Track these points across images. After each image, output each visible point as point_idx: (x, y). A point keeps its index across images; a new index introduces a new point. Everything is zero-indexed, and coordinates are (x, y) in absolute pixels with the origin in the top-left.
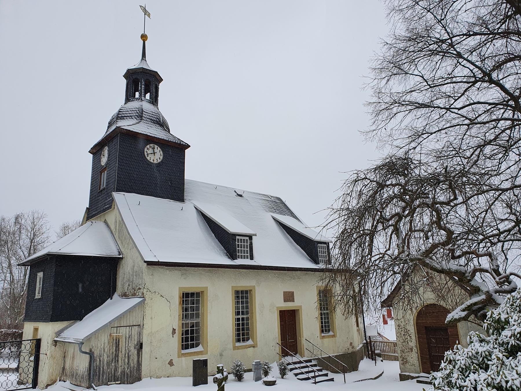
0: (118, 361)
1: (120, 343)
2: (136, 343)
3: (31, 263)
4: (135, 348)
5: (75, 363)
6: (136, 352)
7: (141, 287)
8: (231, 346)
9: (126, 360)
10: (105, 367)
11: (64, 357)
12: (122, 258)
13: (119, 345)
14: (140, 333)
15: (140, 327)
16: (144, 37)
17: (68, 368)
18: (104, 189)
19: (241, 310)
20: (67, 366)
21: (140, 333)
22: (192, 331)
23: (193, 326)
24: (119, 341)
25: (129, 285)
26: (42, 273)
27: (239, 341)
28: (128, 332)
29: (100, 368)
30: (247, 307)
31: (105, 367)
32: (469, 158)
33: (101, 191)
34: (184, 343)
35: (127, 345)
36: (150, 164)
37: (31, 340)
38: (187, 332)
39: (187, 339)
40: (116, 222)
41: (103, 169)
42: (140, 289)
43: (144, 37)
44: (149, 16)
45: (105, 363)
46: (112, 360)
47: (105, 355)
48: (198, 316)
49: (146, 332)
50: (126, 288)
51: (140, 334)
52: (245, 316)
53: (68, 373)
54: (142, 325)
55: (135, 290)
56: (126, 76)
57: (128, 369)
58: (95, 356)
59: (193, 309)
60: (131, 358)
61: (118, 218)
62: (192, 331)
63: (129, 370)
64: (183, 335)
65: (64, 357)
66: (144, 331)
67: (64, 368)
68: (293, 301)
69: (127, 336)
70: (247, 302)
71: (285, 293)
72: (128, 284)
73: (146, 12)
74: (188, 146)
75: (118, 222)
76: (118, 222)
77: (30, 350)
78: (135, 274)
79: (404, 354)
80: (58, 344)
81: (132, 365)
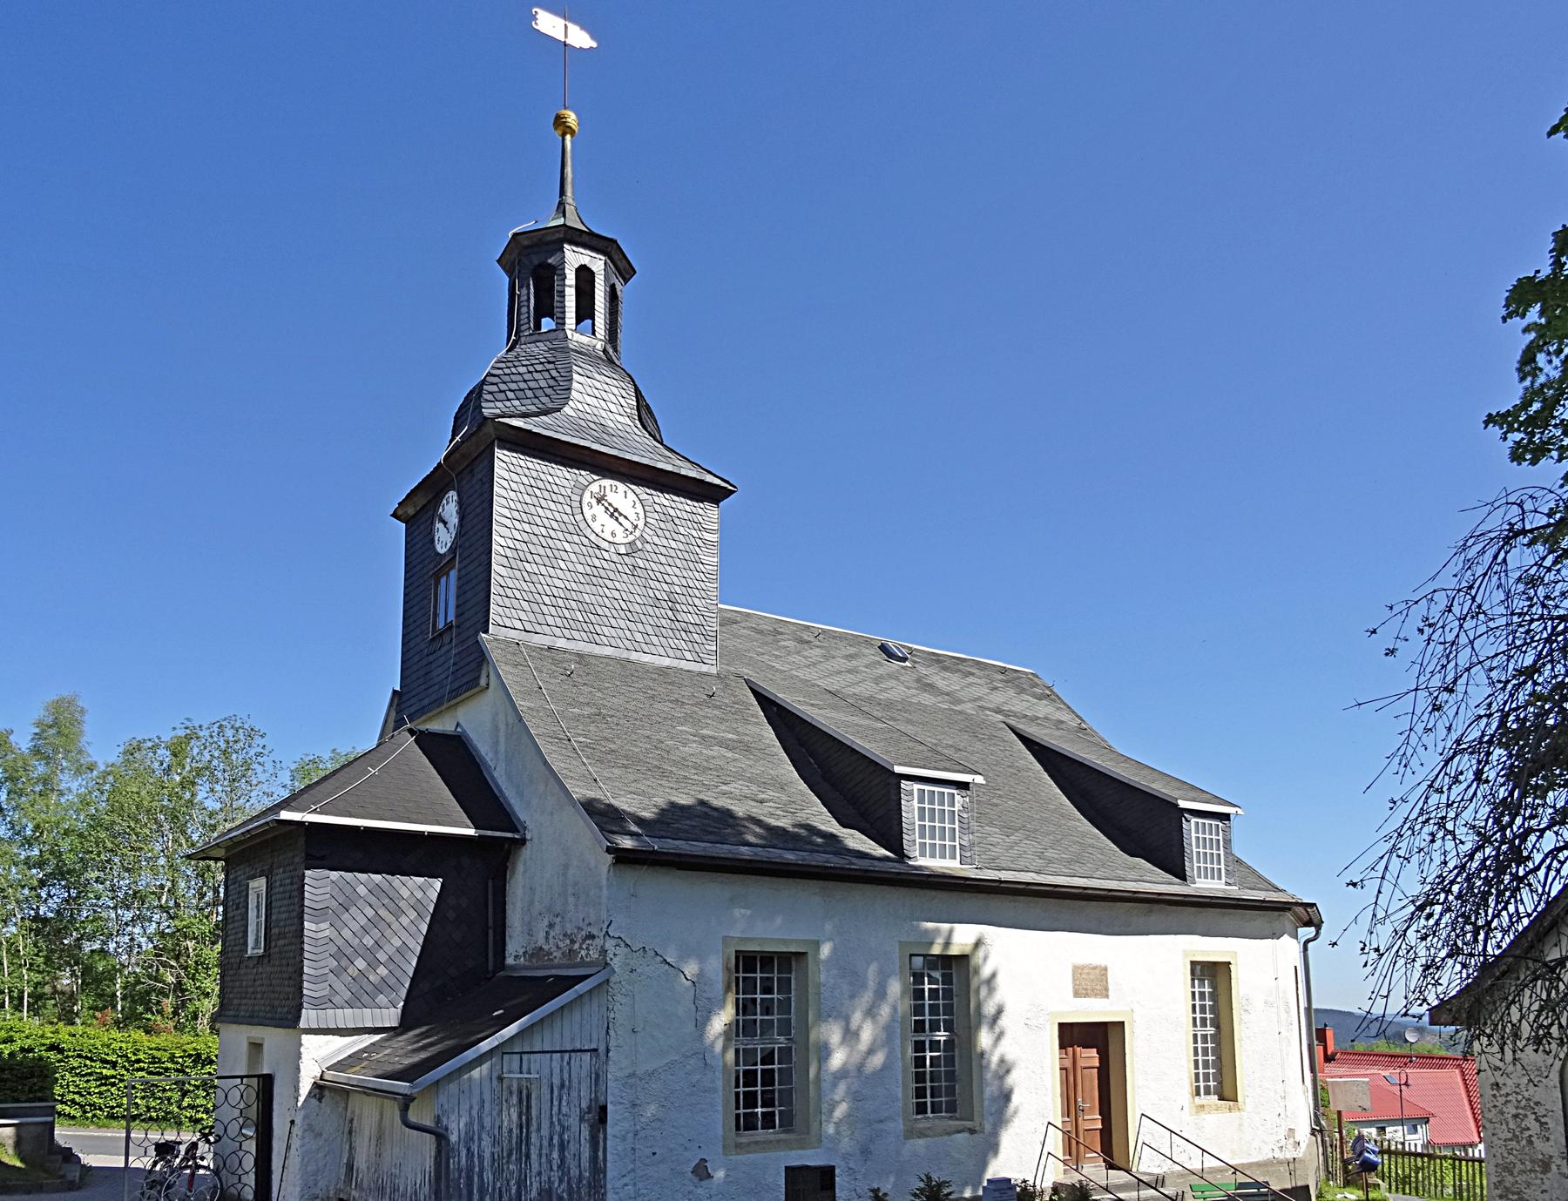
0: (528, 1157)
1: (533, 1103)
2: (584, 1105)
3: (228, 849)
4: (582, 1119)
5: (387, 1156)
6: (586, 1133)
7: (595, 932)
8: (899, 1126)
9: (555, 1155)
10: (488, 1176)
11: (350, 1132)
12: (523, 841)
13: (529, 1107)
14: (597, 1076)
15: (598, 1056)
17: (363, 1166)
18: (449, 627)
19: (927, 1018)
20: (361, 1162)
21: (597, 1076)
22: (768, 1077)
23: (768, 1058)
24: (529, 1097)
25: (551, 926)
26: (262, 882)
27: (921, 1109)
28: (557, 1071)
29: (470, 1179)
31: (488, 1176)
32: (82, 1106)
33: (441, 635)
34: (742, 1111)
35: (555, 1109)
37: (242, 1077)
38: (750, 1078)
39: (750, 1100)
40: (496, 728)
41: (441, 566)
42: (591, 937)
45: (487, 1155)
46: (510, 1155)
47: (484, 1136)
49: (614, 1072)
50: (542, 935)
51: (597, 1078)
53: (365, 1185)
54: (602, 1049)
55: (573, 942)
57: (561, 1181)
58: (453, 1138)
60: (573, 1147)
61: (501, 717)
62: (768, 1077)
63: (564, 1185)
65: (350, 1132)
66: (612, 1068)
67: (350, 1167)
68: (1104, 993)
69: (556, 1081)
71: (1078, 971)
72: (546, 923)
75: (502, 727)
76: (502, 727)
77: (242, 1105)
78: (570, 890)
79: (1511, 1179)
80: (327, 1093)
81: (574, 1172)
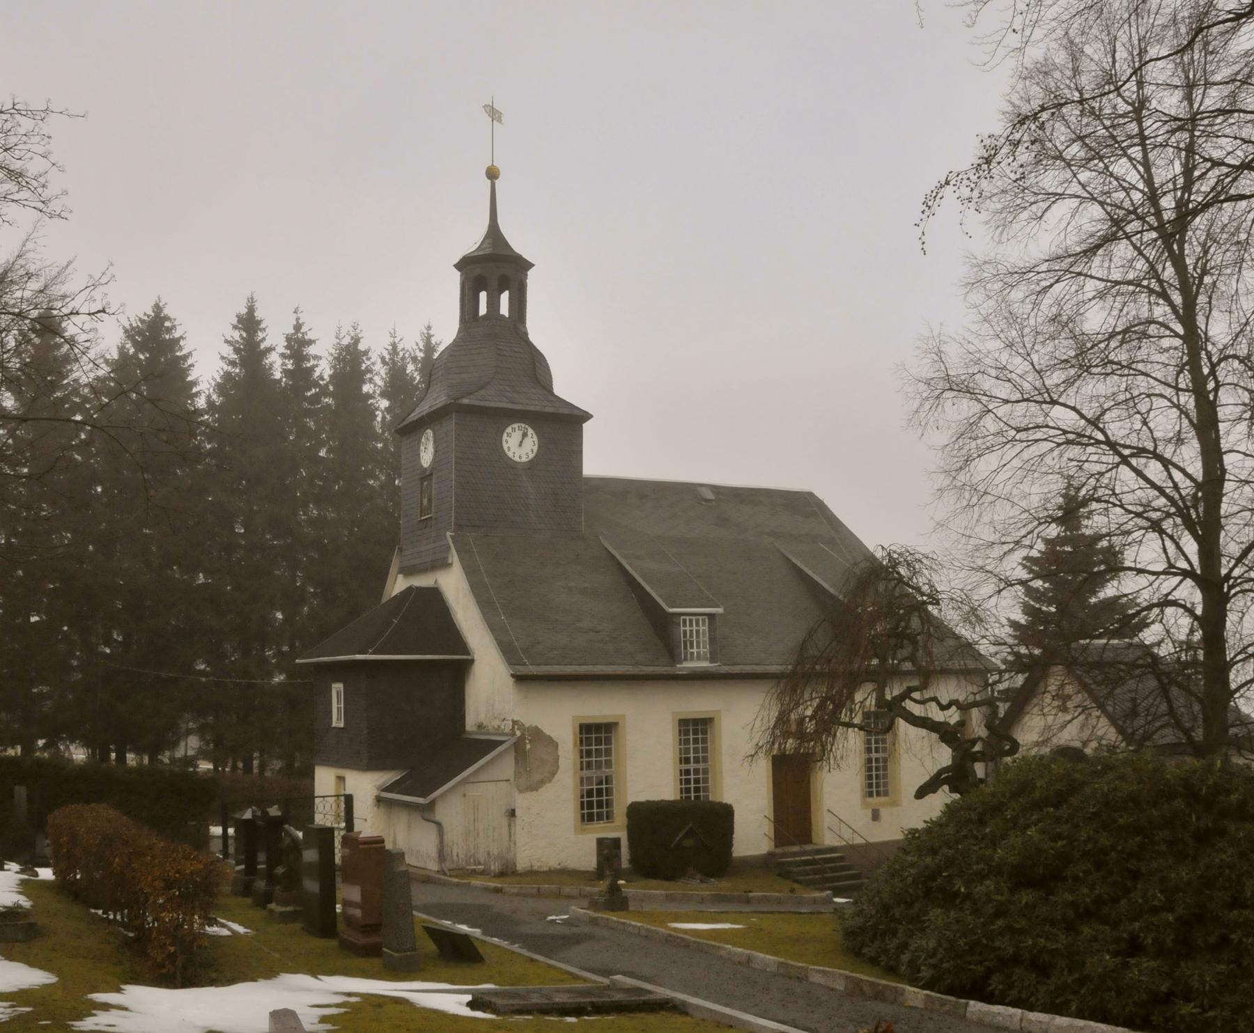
16: (492, 174)
27: (870, 794)
30: (705, 750)
36: (511, 465)
43: (492, 174)
44: (500, 121)
48: (609, 764)
52: (701, 766)
56: (459, 266)
59: (600, 805)
64: (582, 797)
70: (705, 741)
73: (494, 114)
74: (587, 416)
